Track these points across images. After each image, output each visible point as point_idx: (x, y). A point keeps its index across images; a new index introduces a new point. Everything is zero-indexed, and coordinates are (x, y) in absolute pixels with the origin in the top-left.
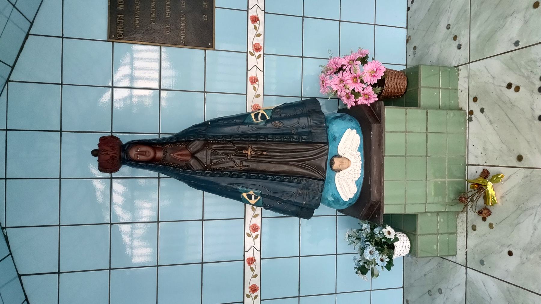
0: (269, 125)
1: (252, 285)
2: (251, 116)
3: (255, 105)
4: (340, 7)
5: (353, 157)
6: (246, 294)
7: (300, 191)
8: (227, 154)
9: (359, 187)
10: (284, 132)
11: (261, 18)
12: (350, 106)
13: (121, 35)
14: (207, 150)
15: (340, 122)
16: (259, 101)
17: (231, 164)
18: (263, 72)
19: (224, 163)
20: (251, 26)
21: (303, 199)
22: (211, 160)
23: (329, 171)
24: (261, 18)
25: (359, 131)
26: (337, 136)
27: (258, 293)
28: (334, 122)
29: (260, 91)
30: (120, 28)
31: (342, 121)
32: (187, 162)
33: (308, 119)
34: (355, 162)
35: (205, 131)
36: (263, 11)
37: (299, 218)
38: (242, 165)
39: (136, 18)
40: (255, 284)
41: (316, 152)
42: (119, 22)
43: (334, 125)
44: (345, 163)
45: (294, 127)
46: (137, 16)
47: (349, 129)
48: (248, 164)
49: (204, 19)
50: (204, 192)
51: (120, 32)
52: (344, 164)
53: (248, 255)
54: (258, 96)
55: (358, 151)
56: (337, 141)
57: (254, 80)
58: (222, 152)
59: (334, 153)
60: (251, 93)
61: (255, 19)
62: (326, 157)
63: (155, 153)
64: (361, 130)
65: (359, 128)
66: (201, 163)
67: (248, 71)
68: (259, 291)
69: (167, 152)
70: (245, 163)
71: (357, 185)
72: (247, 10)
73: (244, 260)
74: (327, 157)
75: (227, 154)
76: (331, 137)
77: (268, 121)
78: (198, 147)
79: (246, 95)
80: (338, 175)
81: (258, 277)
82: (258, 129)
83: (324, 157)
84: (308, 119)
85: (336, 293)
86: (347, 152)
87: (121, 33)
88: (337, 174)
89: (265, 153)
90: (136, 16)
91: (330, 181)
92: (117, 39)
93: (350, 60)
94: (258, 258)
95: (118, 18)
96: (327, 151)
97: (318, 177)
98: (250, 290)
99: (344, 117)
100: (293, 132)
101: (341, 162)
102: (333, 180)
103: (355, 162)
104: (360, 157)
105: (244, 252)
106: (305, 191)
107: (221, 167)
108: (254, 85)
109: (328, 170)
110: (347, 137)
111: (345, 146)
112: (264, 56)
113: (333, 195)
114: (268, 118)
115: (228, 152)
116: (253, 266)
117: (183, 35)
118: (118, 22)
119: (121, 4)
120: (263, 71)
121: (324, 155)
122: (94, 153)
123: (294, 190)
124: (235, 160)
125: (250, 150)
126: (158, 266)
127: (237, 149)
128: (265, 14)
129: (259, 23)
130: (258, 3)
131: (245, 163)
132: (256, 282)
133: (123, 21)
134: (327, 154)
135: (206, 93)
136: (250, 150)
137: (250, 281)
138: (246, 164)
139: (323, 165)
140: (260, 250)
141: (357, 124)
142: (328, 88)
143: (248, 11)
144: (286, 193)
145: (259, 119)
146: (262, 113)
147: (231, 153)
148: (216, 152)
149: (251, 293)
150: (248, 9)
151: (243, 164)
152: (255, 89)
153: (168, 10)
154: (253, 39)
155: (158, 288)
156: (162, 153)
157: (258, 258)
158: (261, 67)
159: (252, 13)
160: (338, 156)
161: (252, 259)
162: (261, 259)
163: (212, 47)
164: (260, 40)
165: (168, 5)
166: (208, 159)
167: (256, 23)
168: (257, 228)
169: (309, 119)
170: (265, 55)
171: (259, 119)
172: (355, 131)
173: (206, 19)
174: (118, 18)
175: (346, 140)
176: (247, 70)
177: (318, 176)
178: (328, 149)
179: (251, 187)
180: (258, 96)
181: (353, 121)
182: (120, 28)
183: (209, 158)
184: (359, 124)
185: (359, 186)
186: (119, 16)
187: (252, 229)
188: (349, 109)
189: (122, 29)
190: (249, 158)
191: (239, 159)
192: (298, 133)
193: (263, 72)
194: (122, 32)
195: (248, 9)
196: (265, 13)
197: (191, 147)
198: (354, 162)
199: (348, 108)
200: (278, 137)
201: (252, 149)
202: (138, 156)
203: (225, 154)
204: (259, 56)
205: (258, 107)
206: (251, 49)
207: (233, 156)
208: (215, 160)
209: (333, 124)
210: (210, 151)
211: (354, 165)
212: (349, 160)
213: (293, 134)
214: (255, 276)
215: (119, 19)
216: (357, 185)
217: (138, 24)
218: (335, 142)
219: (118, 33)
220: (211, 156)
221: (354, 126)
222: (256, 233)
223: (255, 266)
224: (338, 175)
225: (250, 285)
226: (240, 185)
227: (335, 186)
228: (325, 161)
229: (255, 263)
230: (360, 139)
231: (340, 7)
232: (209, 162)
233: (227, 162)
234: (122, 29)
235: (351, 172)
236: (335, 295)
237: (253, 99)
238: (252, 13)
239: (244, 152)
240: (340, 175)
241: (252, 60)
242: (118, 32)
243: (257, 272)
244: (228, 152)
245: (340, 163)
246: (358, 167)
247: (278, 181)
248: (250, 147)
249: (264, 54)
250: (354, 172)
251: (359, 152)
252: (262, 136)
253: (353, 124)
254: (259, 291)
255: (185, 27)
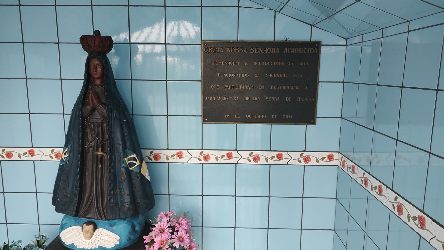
0: (123, 170)
1: (12, 154)
2: (133, 154)
3: (160, 156)
4: (247, 228)
5: (93, 242)
6: (5, 149)
7: (68, 196)
8: (98, 136)
9: (70, 247)
10: (118, 182)
11: (231, 161)
12: (145, 239)
13: (207, 51)
14: (101, 119)
15: (128, 230)
16: (163, 159)
17: (90, 139)
18: (187, 162)
19: (91, 132)
20: (224, 153)
21: (61, 198)
22: (94, 122)
23: (84, 220)
24: (231, 161)
25: (118, 247)
26: (114, 228)
27: (6, 159)
28: (129, 225)
29: (171, 160)
30: (212, 50)
31: (128, 232)
32: (88, 104)
33: (128, 202)
34: (88, 244)
35: (115, 116)
36: (237, 163)
37: (53, 192)
38: (89, 148)
39: (221, 62)
40: (13, 156)
41: (101, 209)
42: (217, 49)
43: (125, 225)
44: (87, 235)
45: (121, 191)
46: (223, 63)
47: (119, 238)
48: (90, 152)
49: (226, 115)
50: (71, 115)
51: (209, 50)
52: (86, 234)
53: (36, 150)
54: (167, 158)
55: (99, 246)
56: (109, 228)
57: (180, 155)
58: (100, 131)
59: (99, 225)
60: (169, 153)
61: (230, 156)
62: (96, 218)
63: (98, 78)
64: (119, 248)
65: (121, 246)
66: (90, 114)
67: (187, 150)
68: (7, 159)
69: (99, 87)
70: (91, 149)
71: (72, 245)
72: (237, 149)
73: (32, 147)
74: (96, 219)
75: (98, 136)
76: (114, 223)
77: (127, 169)
78: (101, 112)
79: (168, 149)
80: (79, 229)
81: (19, 159)
82: (119, 161)
83: (96, 216)
84: (128, 202)
85: (7, 223)
86: (97, 236)
87: (208, 50)
88: (80, 228)
89: (100, 166)
90: (223, 62)
91: (77, 222)
92: (204, 48)
93: (183, 239)
94: (33, 158)
95: (220, 48)
96: (100, 219)
97: (80, 210)
98: (8, 152)
99: (134, 233)
100: (118, 190)
101: (88, 231)
102: (76, 224)
103: (88, 244)
104: (94, 248)
105: (39, 147)
106: (68, 200)
107: (88, 131)
108: (176, 155)
109: (85, 220)
110: (112, 236)
111: (103, 235)
112: (200, 163)
113: (66, 224)
114: (130, 169)
115: (100, 135)
116: (28, 154)
117: (212, 98)
118: (217, 48)
119: (231, 50)
120: (188, 163)
121: (98, 217)
122: (97, 33)
123: (69, 190)
124: (94, 141)
125: (102, 154)
126: (26, 79)
127: (103, 143)
128: (235, 164)
129: (226, 159)
130: (243, 159)
131: (91, 149)
132: (15, 157)
133: (218, 52)
134: (98, 219)
135: (167, 116)
136: (102, 154)
137: (15, 152)
138: (90, 151)
139: (90, 216)
140: (41, 160)
141: (125, 245)
142: (160, 219)
143: (236, 150)
144: (67, 185)
145: (130, 162)
146: (136, 164)
147: (99, 139)
148: (100, 127)
149: (6, 153)
150: (238, 150)
151: (90, 148)
152: (173, 156)
153: (230, 87)
154: (213, 155)
155: (9, 80)
156: (99, 84)
157: (33, 158)
158: (192, 161)
159: (234, 153)
160: (95, 228)
161: (33, 154)
162: (34, 161)
163: (204, 121)
164: (212, 160)
165: (234, 87)
166: (94, 120)
167: (227, 157)
168: (58, 158)
169: (129, 203)
170: (201, 164)
171: (130, 162)
172: (118, 243)
173: (226, 117)
174: (220, 48)
175: (108, 236)
176: (188, 150)
177: (81, 211)
178: (102, 219)
179: (71, 155)
180: (167, 158)
181: (128, 241)
182: (212, 50)
183: (94, 121)
184: (127, 246)
185: (71, 246)
186: (222, 49)
187: (58, 154)
188: (143, 237)
189: (211, 51)
190: (95, 153)
191: (94, 145)
192: (116, 194)
193: (187, 162)
194: (209, 52)
195: (238, 150)
196: (236, 164)
197: (100, 107)
198: (89, 242)
199: (144, 236)
200: (112, 178)
201: (103, 156)
202: (93, 65)
203: (98, 134)
204: (200, 159)
205: (158, 158)
206: (205, 152)
207: (97, 140)
208: (93, 126)
209: (126, 224)
210: (100, 122)
211: (86, 242)
212: (91, 237)
213: (116, 190)
214: (19, 156)
215: (219, 49)
216: (72, 245)
217: (217, 64)
218: (109, 226)
219: (208, 48)
220: (96, 122)
221: (123, 242)
222: (54, 157)
223: (28, 156)
224: (79, 229)
225: (12, 152)
226: (73, 146)
227: (71, 226)
228: (92, 217)
229: (30, 156)
230: (110, 247)
231: (247, 228)
232: (92, 120)
233: (92, 136)
234: (211, 51)
235: (80, 240)
236: (5, 223)
237: (165, 155)
238: (234, 153)
239: (100, 149)
240: (79, 230)
241: (196, 153)
242: (209, 48)
243: (23, 158)
244: (100, 135)
245: (87, 231)
246: (85, 246)
247: (76, 177)
248: (105, 154)
249: (202, 163)
250: (80, 243)
251: (98, 247)
252: (112, 164)
253: (125, 241)
254: (7, 159)
255: (218, 100)
